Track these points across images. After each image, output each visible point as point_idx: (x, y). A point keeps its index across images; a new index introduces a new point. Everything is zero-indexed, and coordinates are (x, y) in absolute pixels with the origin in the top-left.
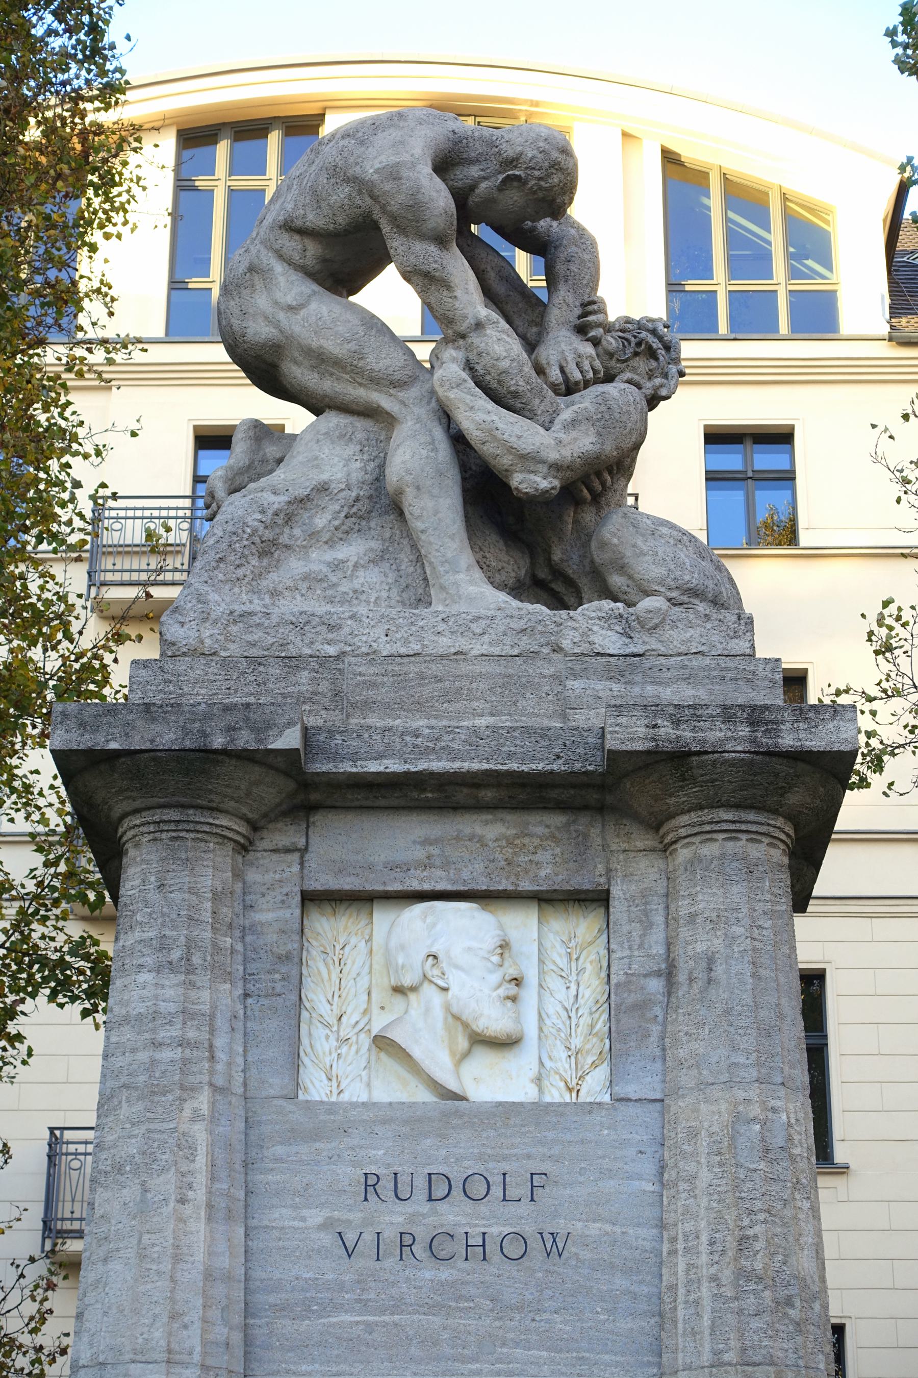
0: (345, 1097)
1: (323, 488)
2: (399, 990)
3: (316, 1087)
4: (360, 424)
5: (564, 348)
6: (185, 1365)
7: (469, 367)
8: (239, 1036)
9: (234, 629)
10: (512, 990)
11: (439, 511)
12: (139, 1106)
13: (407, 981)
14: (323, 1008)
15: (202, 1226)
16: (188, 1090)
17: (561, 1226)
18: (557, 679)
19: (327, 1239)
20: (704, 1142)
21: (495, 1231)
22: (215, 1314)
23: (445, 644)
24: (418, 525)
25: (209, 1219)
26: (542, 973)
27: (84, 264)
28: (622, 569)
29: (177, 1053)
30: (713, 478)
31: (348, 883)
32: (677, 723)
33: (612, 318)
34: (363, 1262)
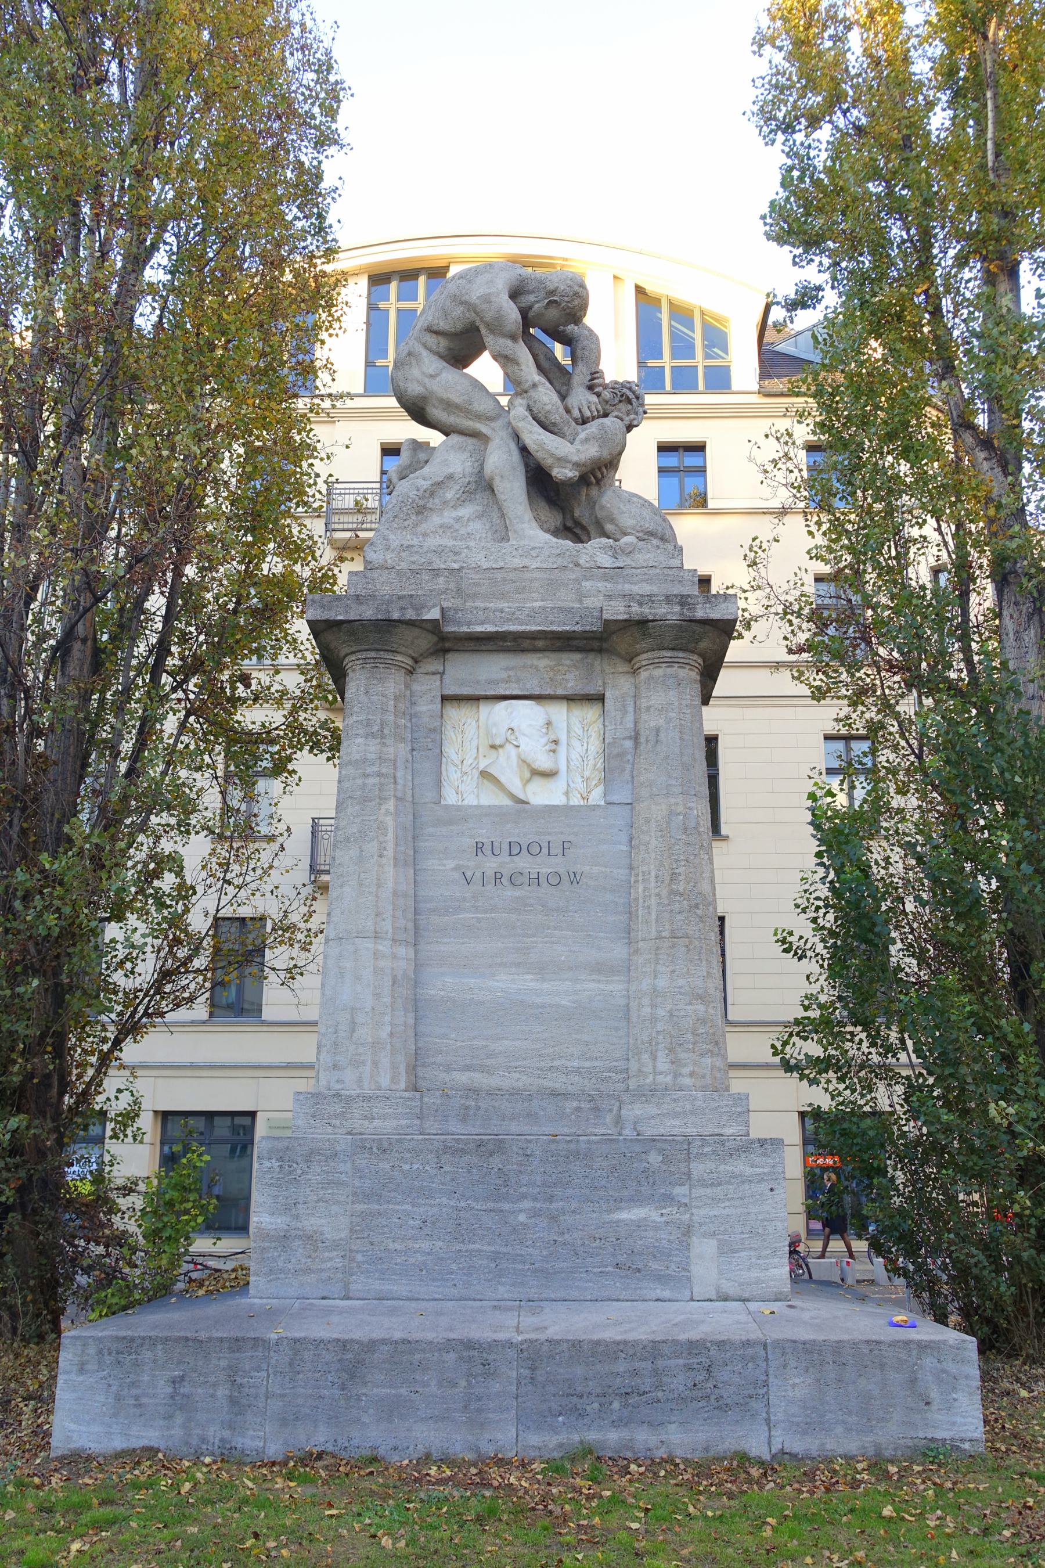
0: (466, 803)
1: (450, 477)
2: (493, 747)
3: (450, 798)
4: (470, 441)
5: (581, 399)
7: (529, 409)
9: (403, 554)
10: (553, 746)
11: (513, 489)
12: (358, 807)
13: (498, 742)
15: (391, 869)
16: (383, 799)
17: (578, 868)
18: (577, 581)
19: (457, 875)
20: (653, 824)
21: (544, 871)
22: (399, 913)
23: (517, 562)
25: (395, 865)
26: (569, 737)
28: (612, 521)
32: (641, 604)
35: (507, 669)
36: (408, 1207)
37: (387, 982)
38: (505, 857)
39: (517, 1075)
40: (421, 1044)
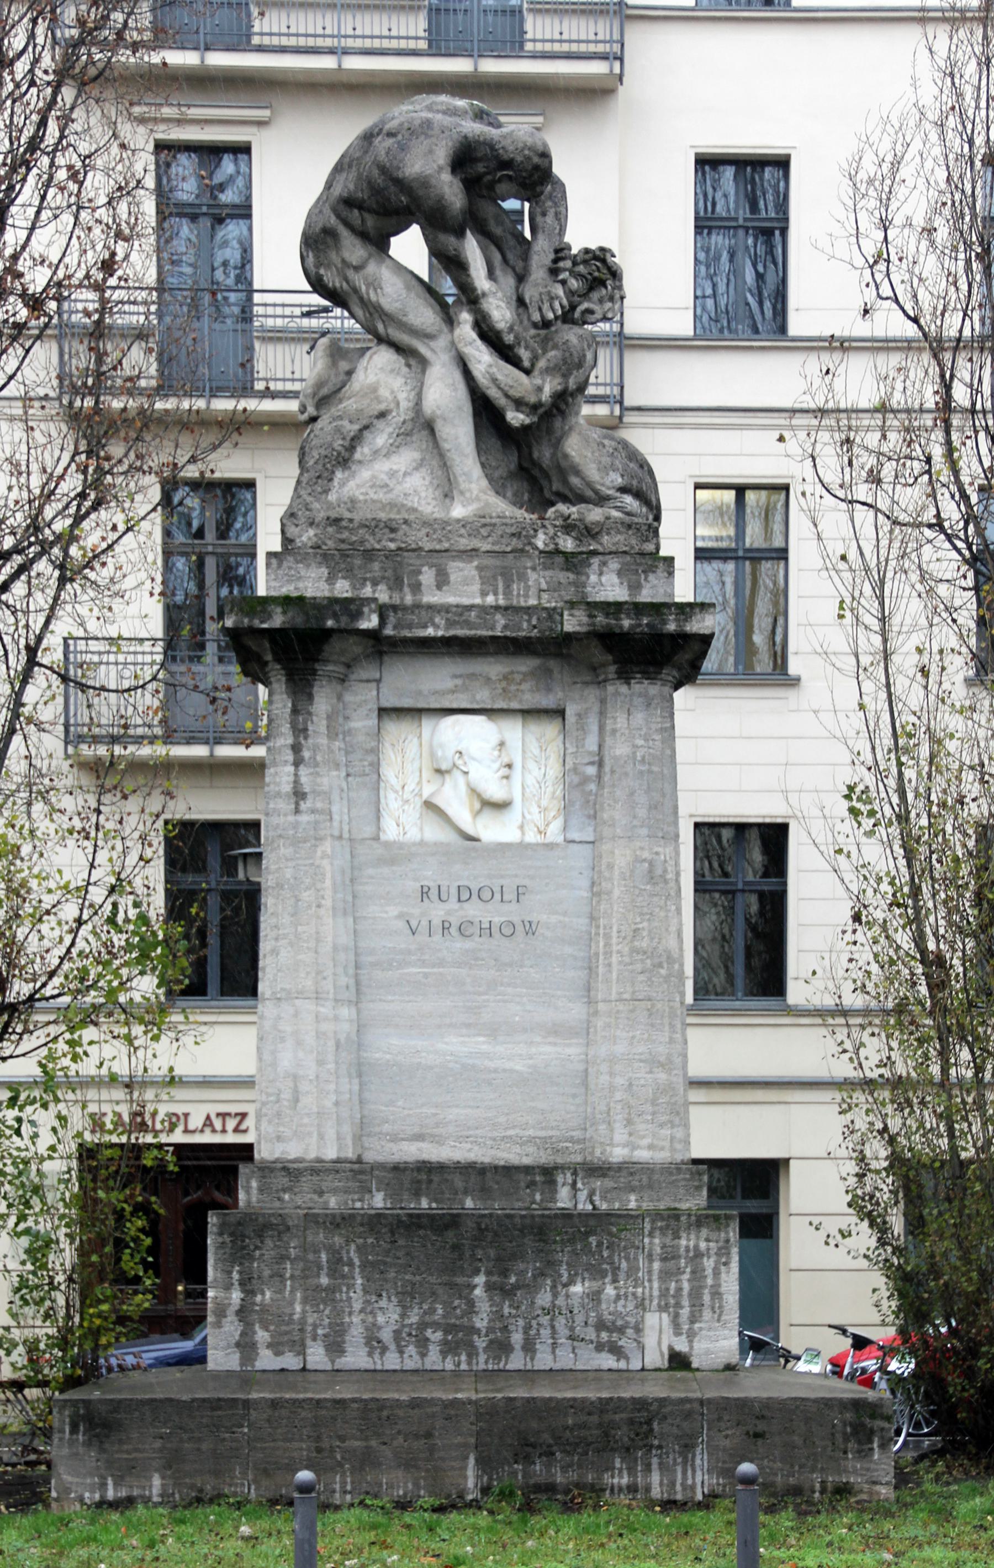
2: (439, 771)
3: (391, 832)
6: (326, 999)
8: (345, 802)
10: (505, 771)
11: (459, 433)
12: (291, 850)
13: (444, 767)
14: (393, 781)
15: (330, 921)
17: (534, 917)
19: (401, 924)
20: (616, 872)
21: (497, 920)
22: (340, 970)
24: (446, 446)
25: (334, 916)
26: (524, 758)
28: (578, 473)
31: (407, 703)
32: (607, 615)
33: (574, 251)
34: (422, 938)
35: (455, 676)
37: (331, 1044)
38: (453, 904)
39: (469, 1146)
40: (366, 1113)
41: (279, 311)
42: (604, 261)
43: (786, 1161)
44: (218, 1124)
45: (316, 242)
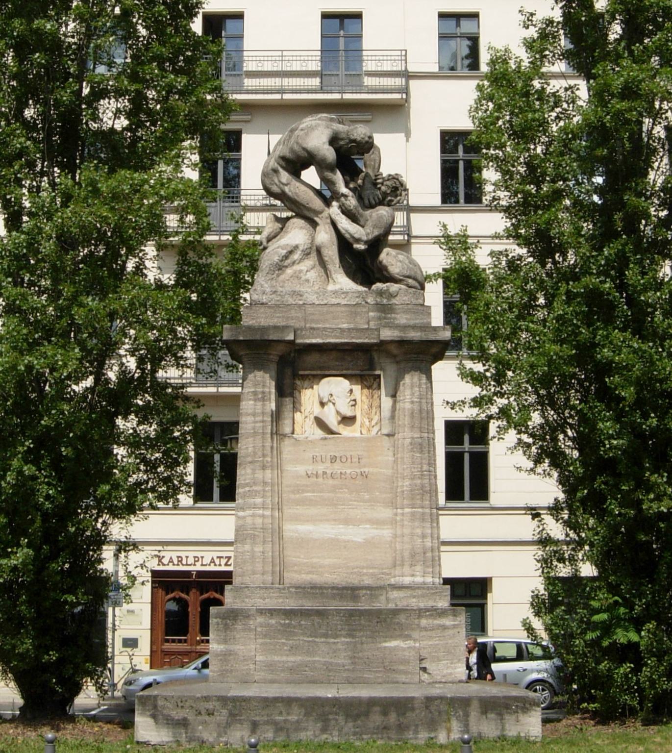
1: (297, 247)
7: (340, 207)
11: (332, 253)
24: (326, 259)
27: (244, 221)
29: (261, 424)
30: (442, 37)
36: (283, 641)
38: (328, 464)
41: (253, 198)
42: (398, 179)
43: (491, 579)
44: (217, 561)
45: (267, 175)
